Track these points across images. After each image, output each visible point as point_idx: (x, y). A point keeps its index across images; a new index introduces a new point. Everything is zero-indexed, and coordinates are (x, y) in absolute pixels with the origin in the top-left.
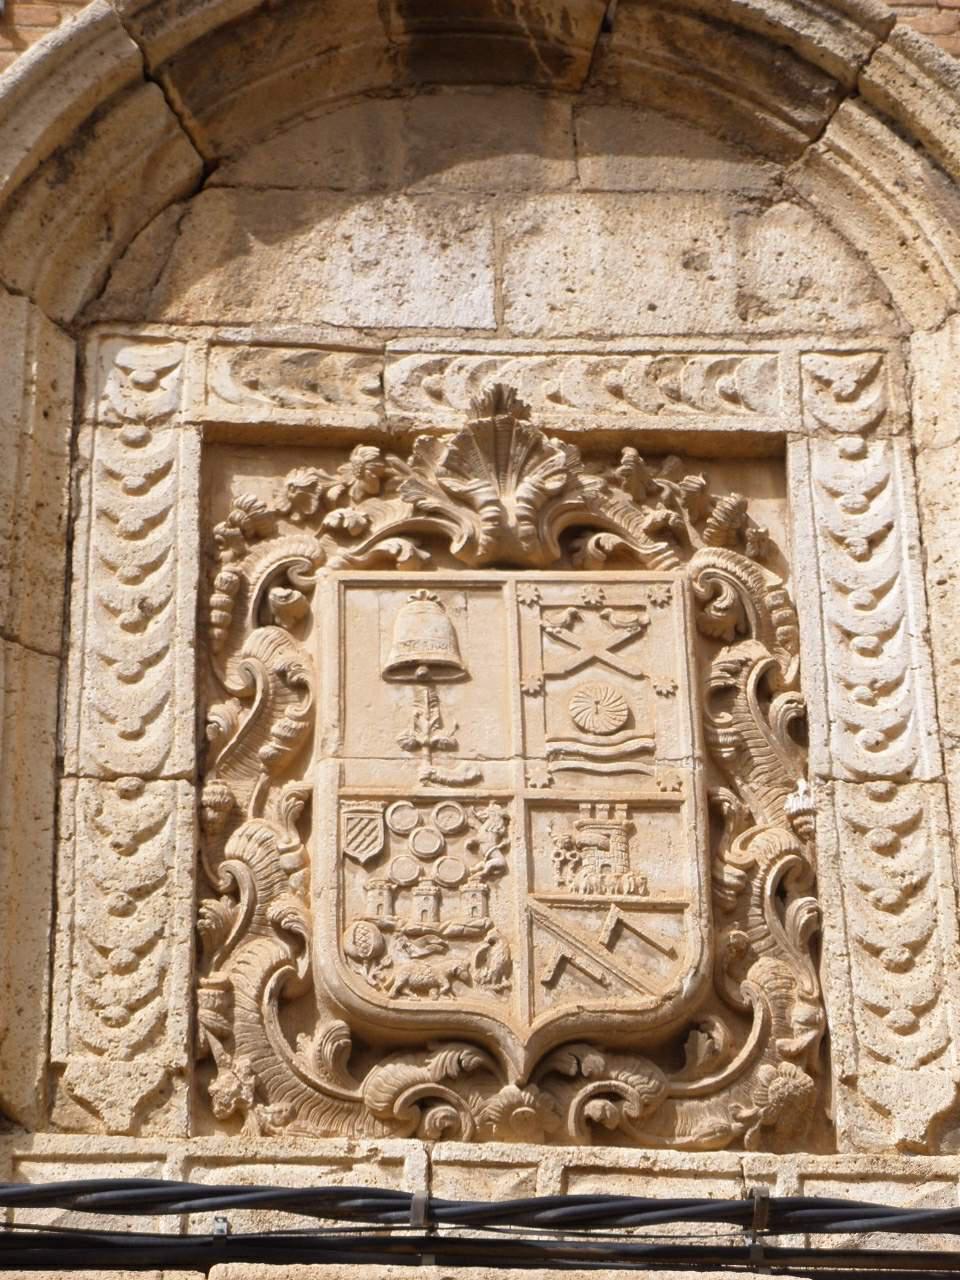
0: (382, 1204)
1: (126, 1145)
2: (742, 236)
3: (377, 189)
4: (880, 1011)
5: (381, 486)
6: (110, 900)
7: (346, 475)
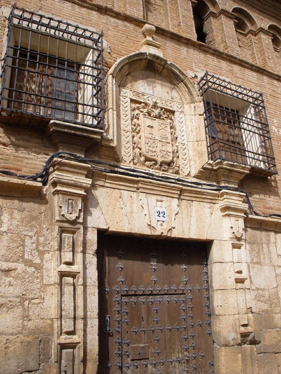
0: (152, 175)
1: (128, 165)
2: (171, 92)
3: (143, 79)
4: (184, 164)
5: (144, 108)
6: (126, 142)
7: (141, 106)
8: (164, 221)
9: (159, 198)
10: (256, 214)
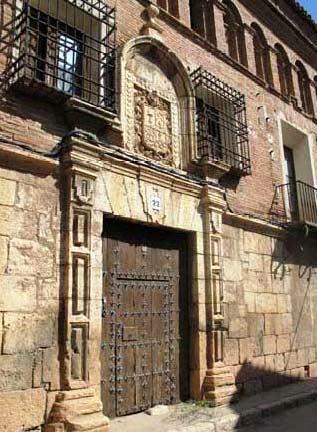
9: (155, 186)
10: (231, 211)
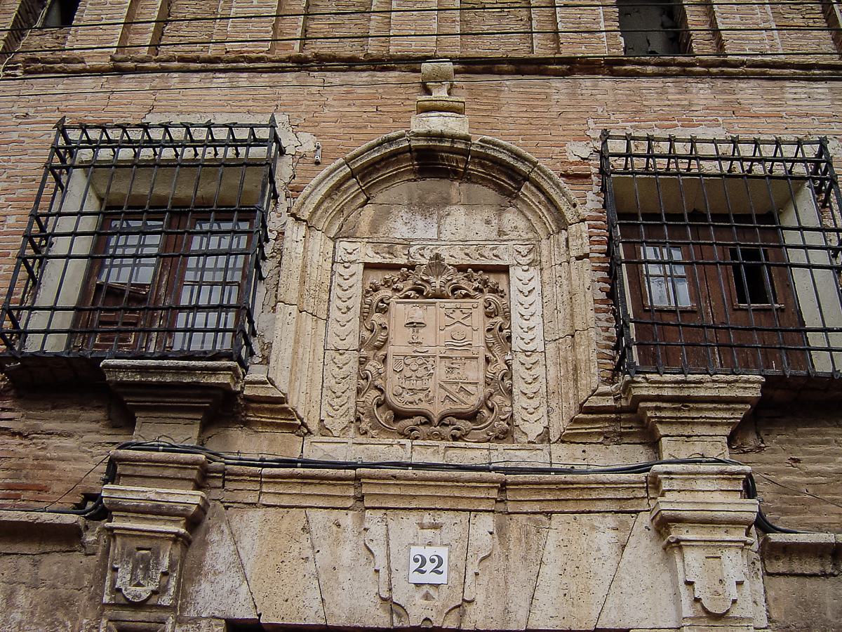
8: (437, 586)
9: (427, 518)
